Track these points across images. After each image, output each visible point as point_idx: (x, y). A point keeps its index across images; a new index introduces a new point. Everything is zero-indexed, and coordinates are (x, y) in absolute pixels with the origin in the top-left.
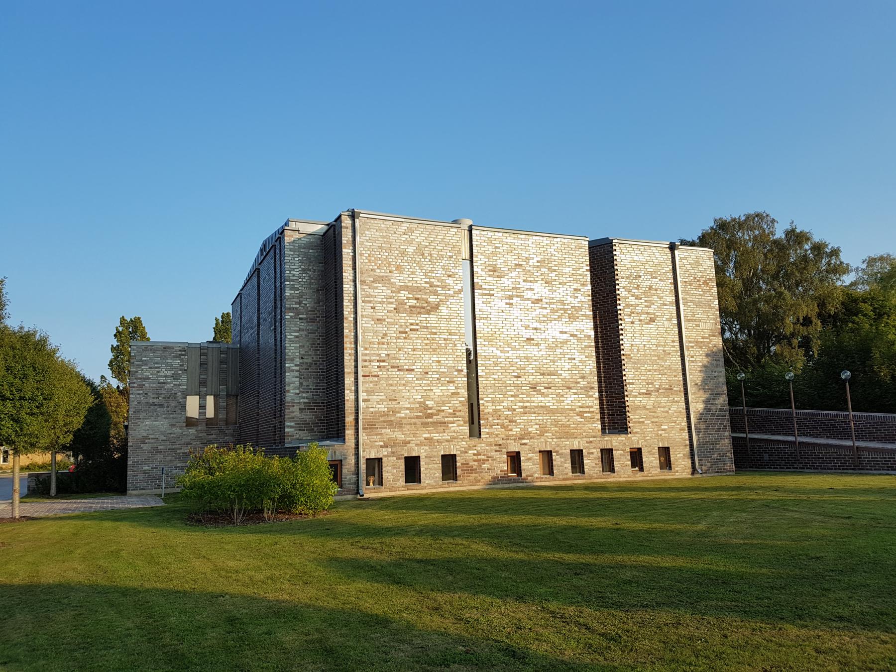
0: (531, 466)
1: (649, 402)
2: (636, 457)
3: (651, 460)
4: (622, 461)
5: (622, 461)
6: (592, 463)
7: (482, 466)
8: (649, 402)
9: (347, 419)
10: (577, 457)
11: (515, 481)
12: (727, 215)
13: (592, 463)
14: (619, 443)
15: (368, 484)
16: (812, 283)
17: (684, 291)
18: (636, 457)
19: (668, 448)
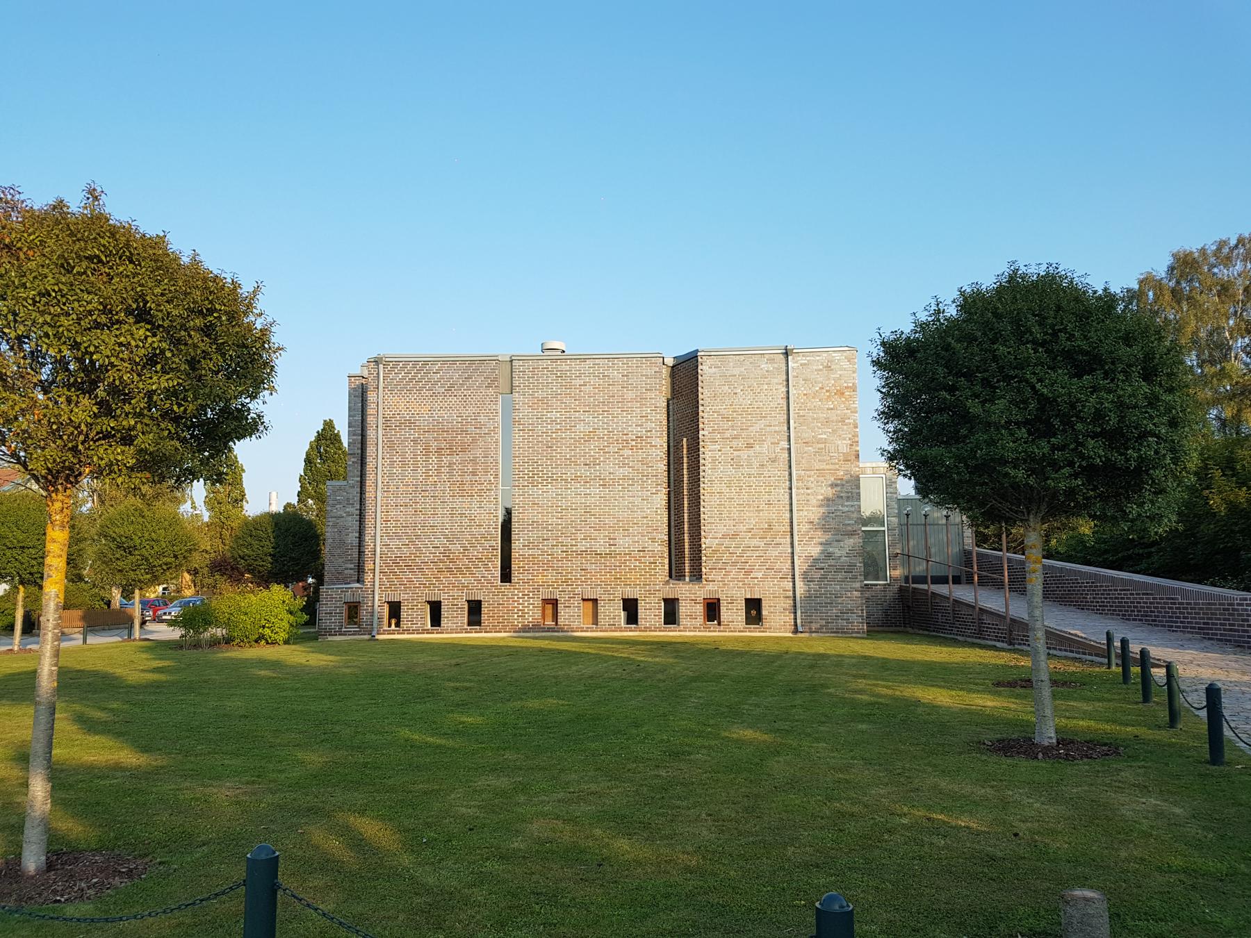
0: (573, 617)
1: (527, 552)
2: (712, 610)
3: (733, 614)
4: (692, 612)
5: (692, 612)
6: (651, 613)
7: (512, 616)
8: (527, 552)
9: (944, 692)
10: (631, 609)
11: (549, 630)
12: (1193, 245)
13: (651, 613)
14: (690, 596)
15: (390, 626)
16: (147, 560)
17: (797, 438)
18: (712, 610)
19: (760, 600)
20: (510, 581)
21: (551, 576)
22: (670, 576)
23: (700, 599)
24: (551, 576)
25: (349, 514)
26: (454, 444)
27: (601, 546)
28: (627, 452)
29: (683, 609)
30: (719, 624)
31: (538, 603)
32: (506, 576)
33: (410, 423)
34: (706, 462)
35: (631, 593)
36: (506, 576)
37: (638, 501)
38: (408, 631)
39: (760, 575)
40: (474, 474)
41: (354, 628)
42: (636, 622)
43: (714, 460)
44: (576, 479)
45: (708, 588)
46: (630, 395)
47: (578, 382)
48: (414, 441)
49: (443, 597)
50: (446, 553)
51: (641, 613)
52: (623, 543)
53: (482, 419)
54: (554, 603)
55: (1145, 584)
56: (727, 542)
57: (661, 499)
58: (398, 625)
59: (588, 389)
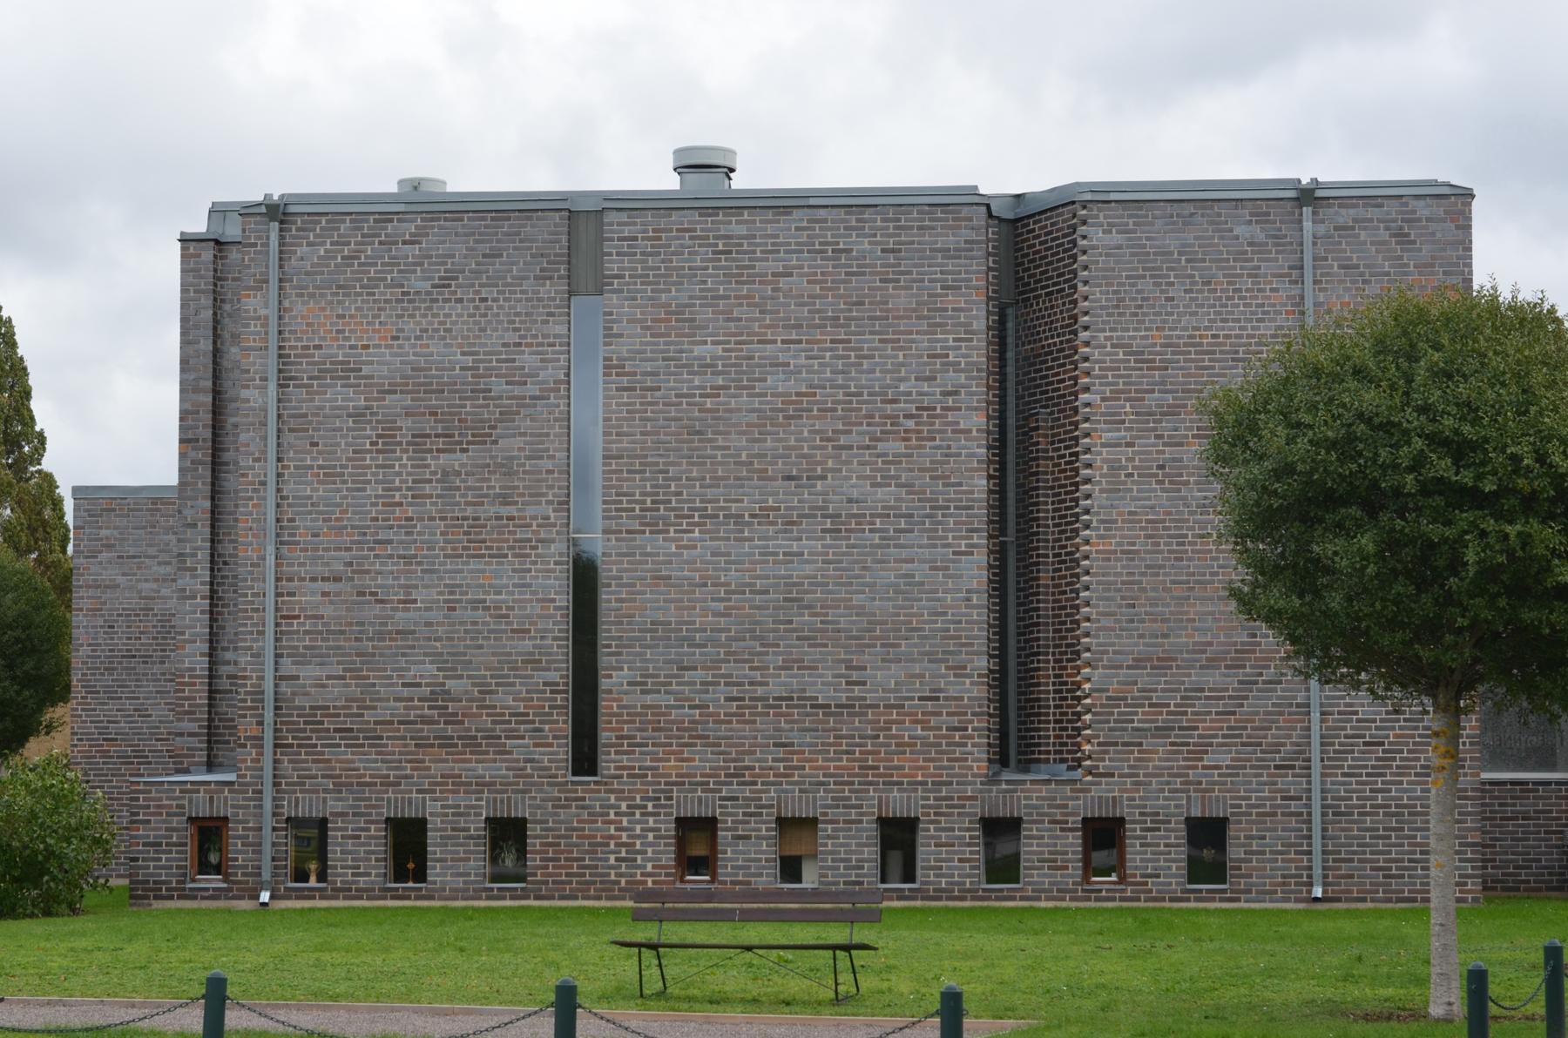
8: (638, 700)
20: (593, 771)
21: (701, 761)
22: (1004, 761)
23: (1075, 821)
24: (701, 761)
25: (184, 595)
26: (454, 420)
27: (824, 685)
28: (894, 447)
29: (1032, 846)
30: (1122, 880)
31: (668, 828)
32: (585, 759)
33: (348, 371)
34: (1096, 475)
35: (899, 803)
36: (585, 759)
37: (920, 572)
38: (345, 892)
39: (1225, 759)
40: (505, 500)
41: (214, 881)
42: (420, 876)
43: (1115, 467)
44: (763, 515)
45: (1094, 792)
46: (901, 300)
47: (773, 266)
48: (358, 415)
49: (433, 810)
50: (438, 696)
51: (925, 852)
52: (884, 678)
53: (527, 359)
54: (707, 826)
55: (758, 910)
56: (1144, 677)
57: (975, 571)
58: (909, 876)
59: (797, 283)
